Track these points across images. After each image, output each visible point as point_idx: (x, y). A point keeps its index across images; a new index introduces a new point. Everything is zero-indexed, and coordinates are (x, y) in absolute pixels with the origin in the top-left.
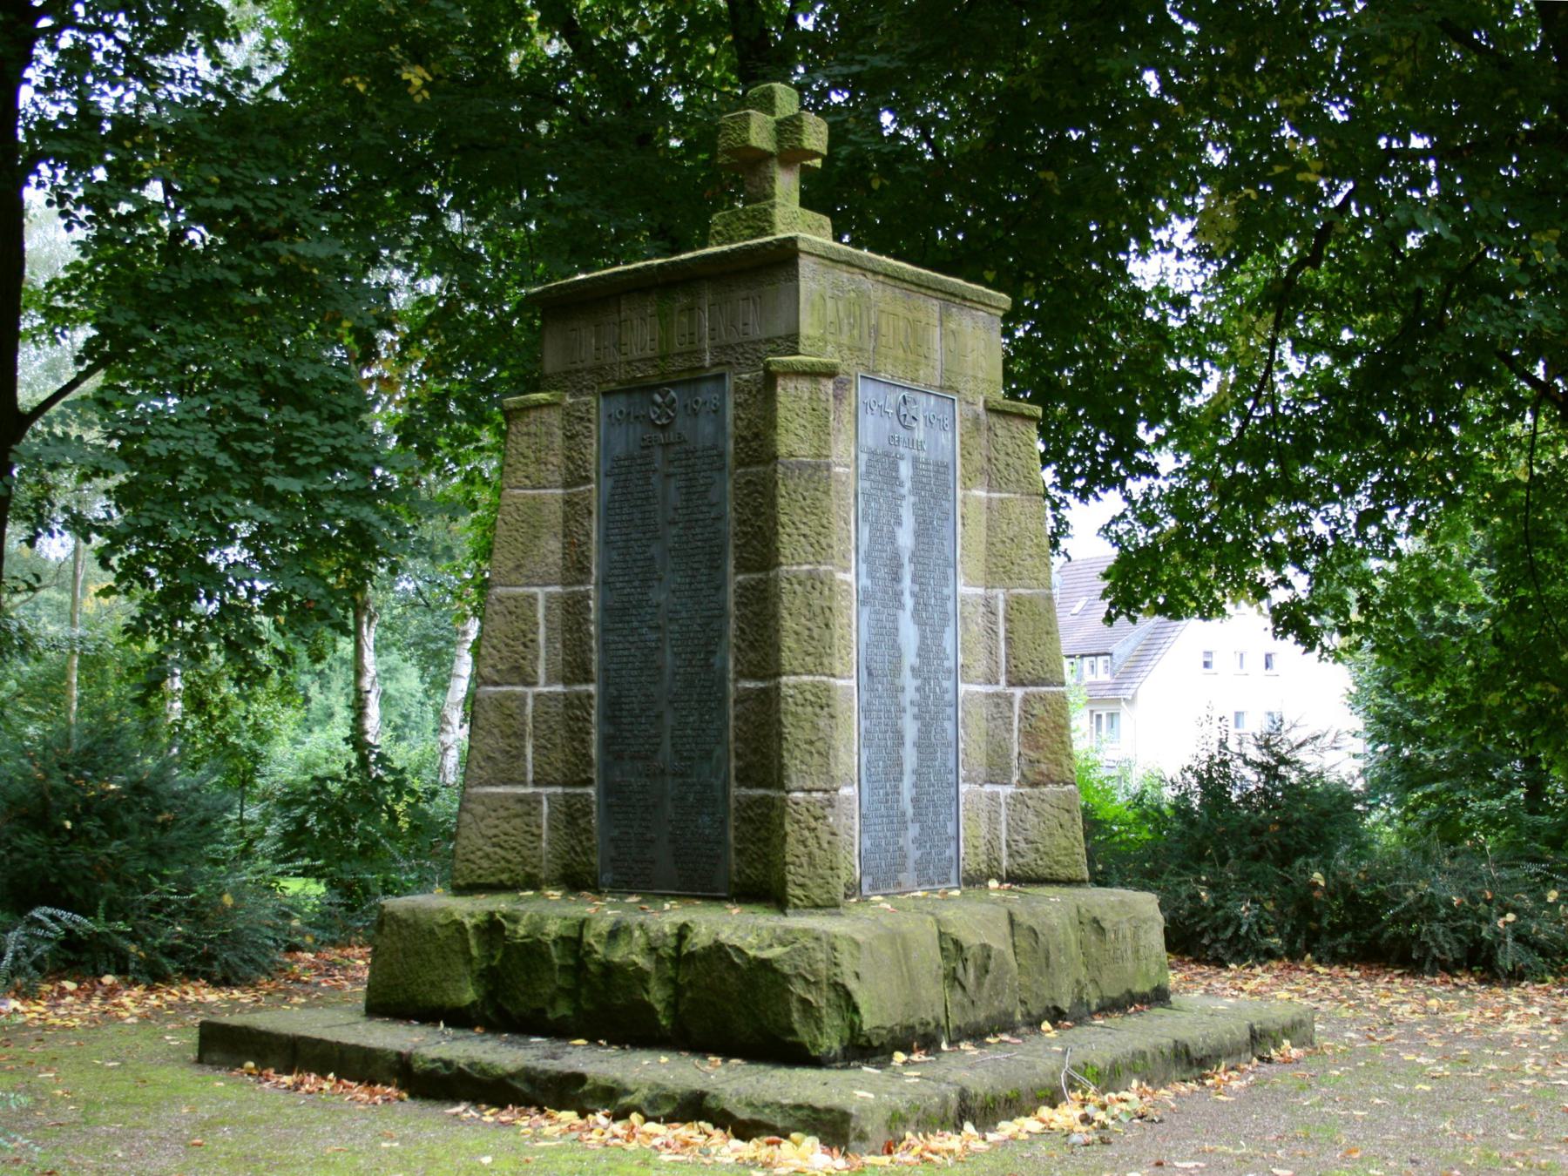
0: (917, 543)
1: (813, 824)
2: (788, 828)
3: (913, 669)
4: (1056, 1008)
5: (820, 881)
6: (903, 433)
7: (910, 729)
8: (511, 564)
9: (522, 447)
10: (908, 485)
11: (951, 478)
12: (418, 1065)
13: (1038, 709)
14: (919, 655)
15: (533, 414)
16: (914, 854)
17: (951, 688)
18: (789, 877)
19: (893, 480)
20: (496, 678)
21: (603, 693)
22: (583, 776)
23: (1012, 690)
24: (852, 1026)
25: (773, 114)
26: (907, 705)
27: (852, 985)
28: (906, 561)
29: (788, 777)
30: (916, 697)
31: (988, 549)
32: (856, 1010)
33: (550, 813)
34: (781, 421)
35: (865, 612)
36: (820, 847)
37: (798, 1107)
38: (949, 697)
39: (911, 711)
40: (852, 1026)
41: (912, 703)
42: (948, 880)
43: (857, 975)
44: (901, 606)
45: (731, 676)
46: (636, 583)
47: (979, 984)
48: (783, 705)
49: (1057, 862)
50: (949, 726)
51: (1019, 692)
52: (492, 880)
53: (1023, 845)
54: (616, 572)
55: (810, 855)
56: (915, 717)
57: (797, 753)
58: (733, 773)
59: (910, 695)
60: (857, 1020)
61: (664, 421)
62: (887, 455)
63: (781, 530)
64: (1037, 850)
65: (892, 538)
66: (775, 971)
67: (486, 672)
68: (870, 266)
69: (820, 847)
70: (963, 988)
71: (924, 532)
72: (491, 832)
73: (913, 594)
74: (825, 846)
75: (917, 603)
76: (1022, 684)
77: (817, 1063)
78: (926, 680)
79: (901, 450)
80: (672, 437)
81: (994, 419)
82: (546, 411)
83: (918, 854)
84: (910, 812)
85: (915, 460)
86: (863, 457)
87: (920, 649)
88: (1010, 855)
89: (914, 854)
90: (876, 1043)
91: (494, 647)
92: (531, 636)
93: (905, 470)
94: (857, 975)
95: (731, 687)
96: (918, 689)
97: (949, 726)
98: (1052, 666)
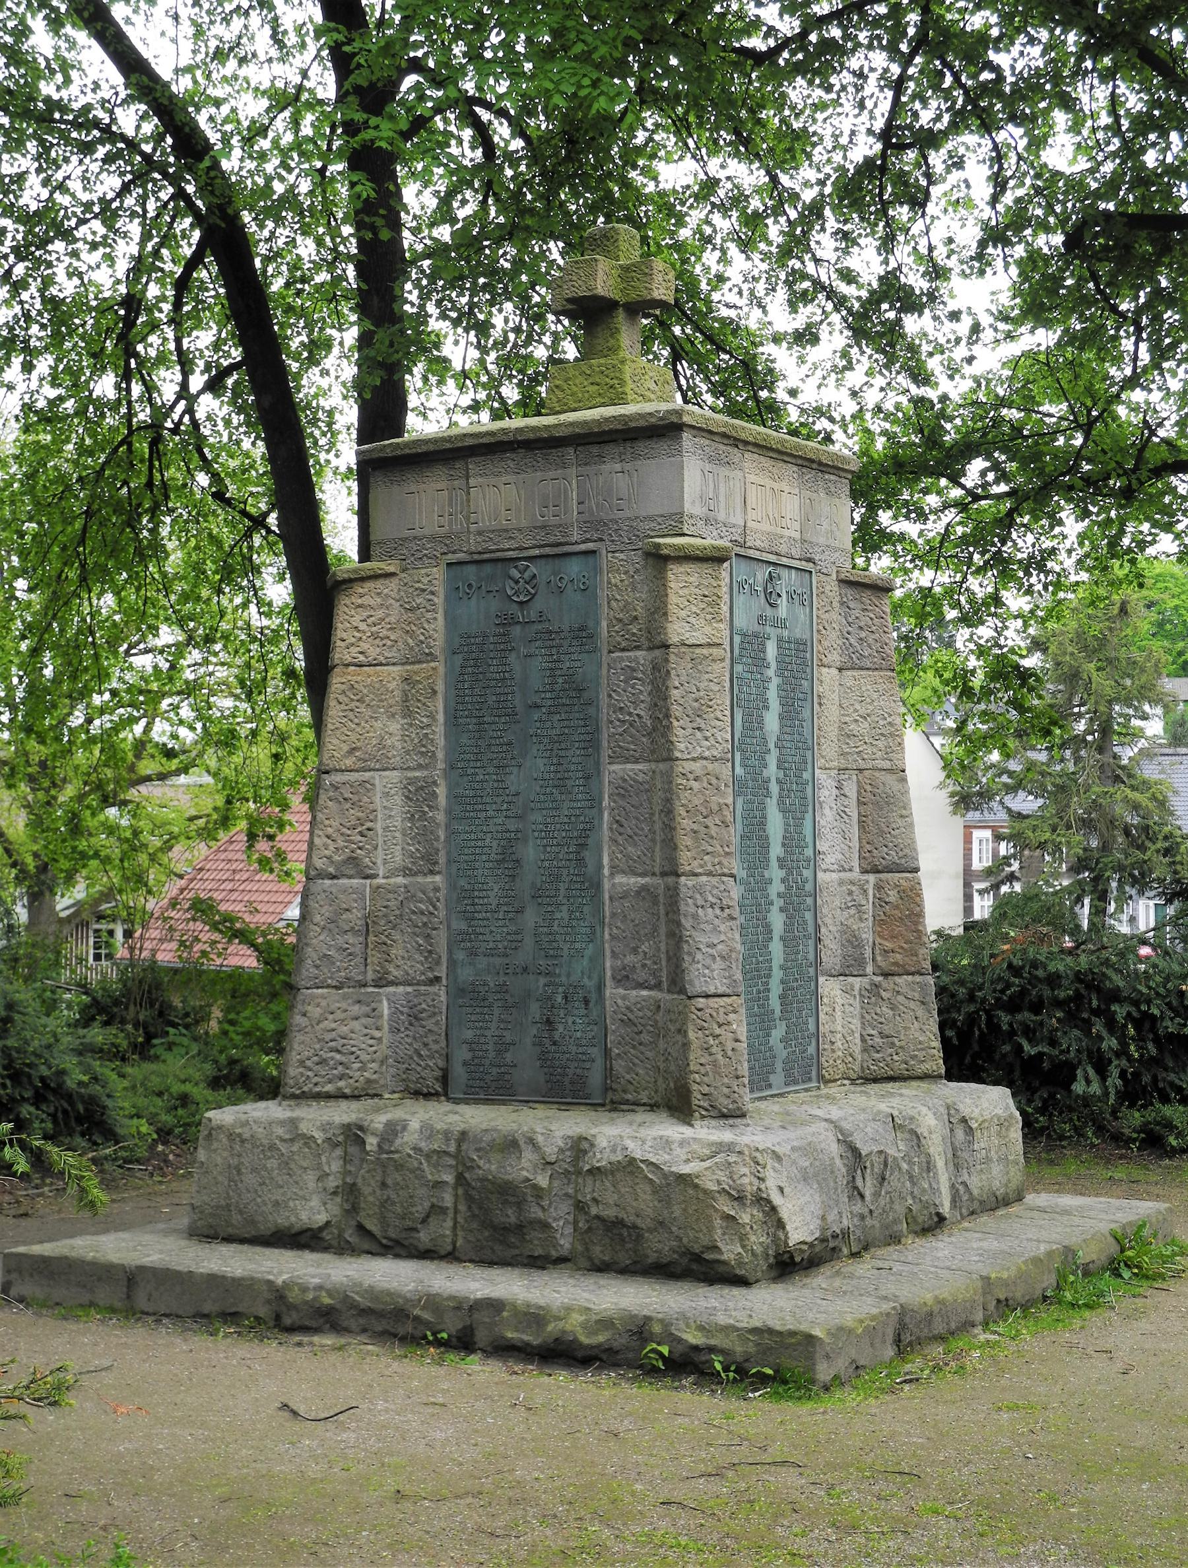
0: (782, 726)
1: (718, 1031)
2: (692, 1035)
3: (779, 859)
4: (938, 1214)
5: (726, 1091)
6: (769, 612)
7: (777, 920)
8: (346, 748)
9: (356, 621)
10: (773, 665)
11: (808, 655)
12: (293, 1296)
13: (893, 896)
14: (784, 845)
15: (369, 585)
16: (782, 1053)
17: (811, 878)
18: (695, 1087)
19: (760, 662)
20: (331, 870)
21: (452, 886)
22: (430, 975)
23: (866, 877)
24: (776, 1239)
25: (617, 259)
26: (773, 896)
27: (777, 1199)
28: (772, 746)
29: (691, 982)
30: (782, 889)
31: (841, 729)
32: (781, 1225)
33: (391, 1015)
34: (672, 608)
35: (740, 801)
36: (725, 1056)
37: (754, 1331)
38: (809, 887)
39: (779, 903)
40: (776, 1239)
41: (779, 895)
42: (810, 1080)
43: (781, 1189)
44: (768, 795)
45: (606, 872)
46: (491, 770)
47: (877, 1194)
48: (683, 907)
49: (914, 1057)
50: (808, 916)
51: (872, 878)
52: (329, 1088)
53: (878, 1040)
54: (467, 757)
55: (715, 1064)
56: (781, 910)
57: (699, 956)
58: (609, 973)
59: (776, 888)
60: (781, 1235)
61: (522, 598)
62: (756, 635)
63: (675, 723)
64: (893, 1045)
65: (761, 722)
66: (696, 1186)
67: (319, 863)
68: (743, 436)
69: (725, 1056)
70: (862, 1196)
71: (789, 715)
72: (328, 1037)
73: (779, 781)
74: (730, 1053)
75: (782, 789)
76: (876, 870)
77: (742, 1282)
78: (790, 872)
79: (768, 629)
80: (533, 616)
81: (850, 592)
82: (382, 581)
83: (785, 1053)
84: (778, 1009)
85: (780, 640)
86: (737, 639)
87: (785, 837)
88: (864, 1050)
89: (782, 1053)
90: (798, 1259)
91: (328, 837)
92: (369, 824)
93: (771, 650)
94: (781, 1189)
95: (606, 885)
96: (783, 881)
97: (808, 916)
98: (906, 851)
